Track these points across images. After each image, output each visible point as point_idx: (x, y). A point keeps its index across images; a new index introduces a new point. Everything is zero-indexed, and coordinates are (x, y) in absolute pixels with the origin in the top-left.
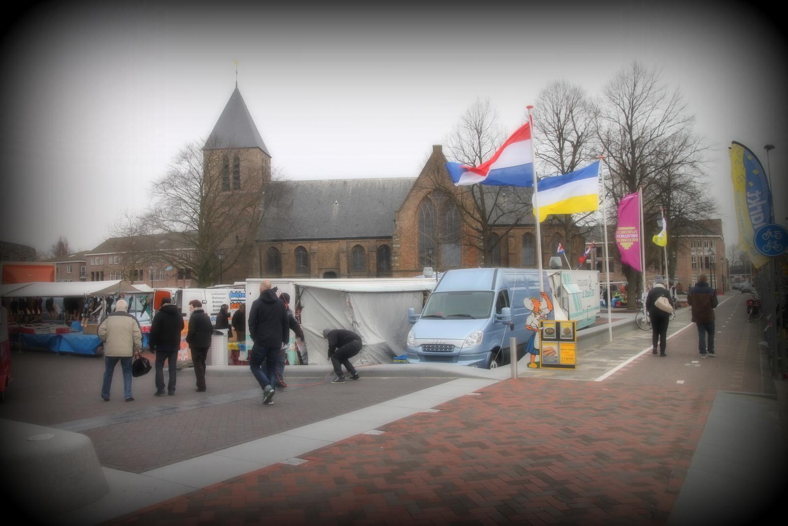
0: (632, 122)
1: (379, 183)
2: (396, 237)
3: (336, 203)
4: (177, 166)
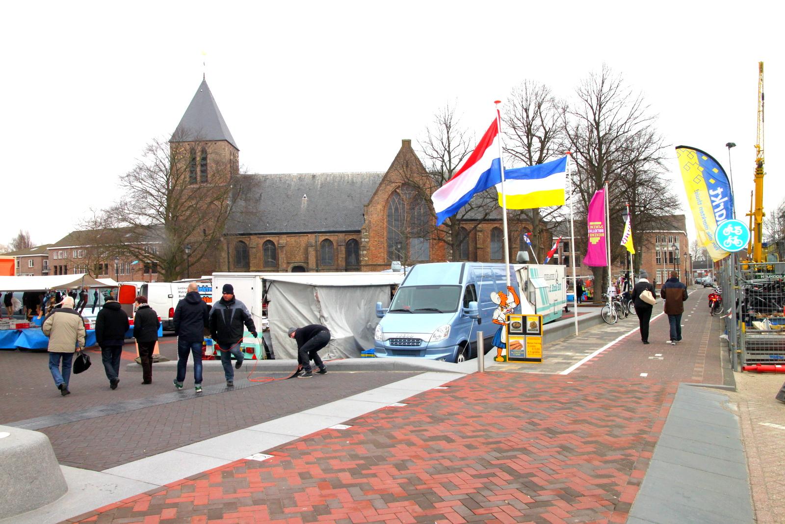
1: (348, 177)
2: (365, 231)
3: (305, 197)
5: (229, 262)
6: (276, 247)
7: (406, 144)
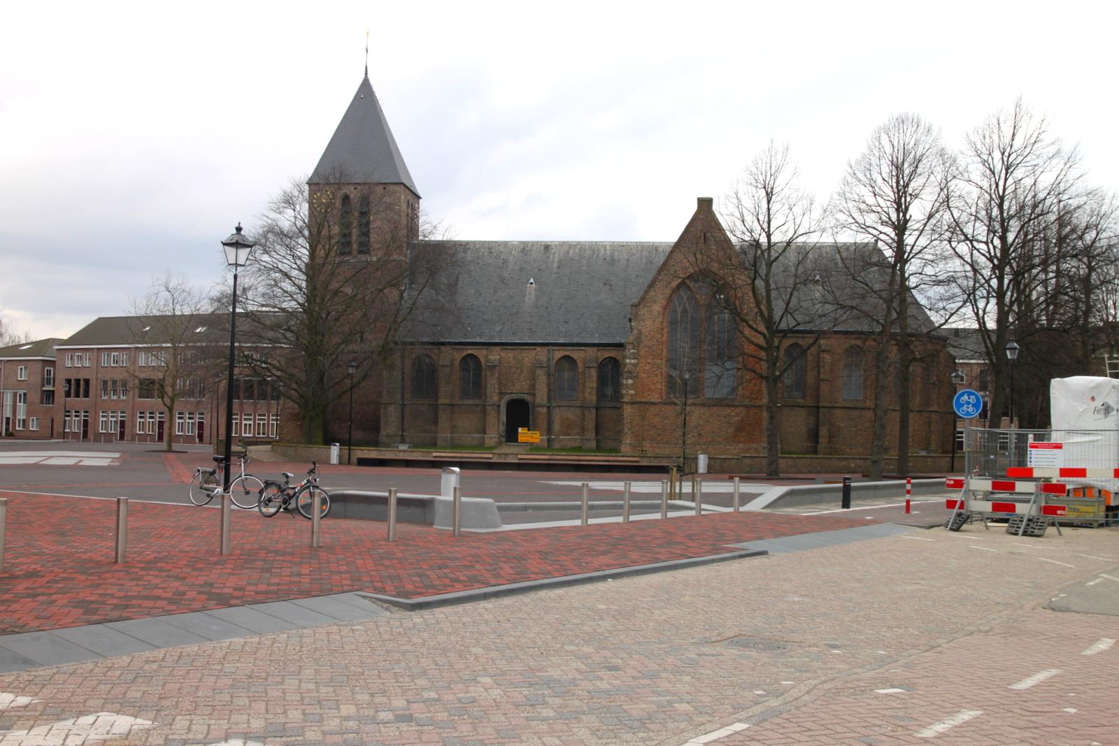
0: (1004, 190)
1: (606, 250)
2: (631, 347)
4: (273, 215)
5: (403, 388)
6: (483, 365)
7: (705, 205)
